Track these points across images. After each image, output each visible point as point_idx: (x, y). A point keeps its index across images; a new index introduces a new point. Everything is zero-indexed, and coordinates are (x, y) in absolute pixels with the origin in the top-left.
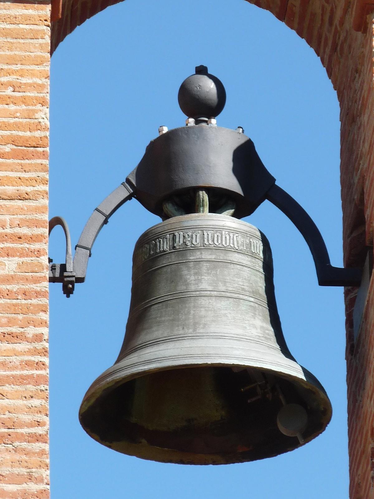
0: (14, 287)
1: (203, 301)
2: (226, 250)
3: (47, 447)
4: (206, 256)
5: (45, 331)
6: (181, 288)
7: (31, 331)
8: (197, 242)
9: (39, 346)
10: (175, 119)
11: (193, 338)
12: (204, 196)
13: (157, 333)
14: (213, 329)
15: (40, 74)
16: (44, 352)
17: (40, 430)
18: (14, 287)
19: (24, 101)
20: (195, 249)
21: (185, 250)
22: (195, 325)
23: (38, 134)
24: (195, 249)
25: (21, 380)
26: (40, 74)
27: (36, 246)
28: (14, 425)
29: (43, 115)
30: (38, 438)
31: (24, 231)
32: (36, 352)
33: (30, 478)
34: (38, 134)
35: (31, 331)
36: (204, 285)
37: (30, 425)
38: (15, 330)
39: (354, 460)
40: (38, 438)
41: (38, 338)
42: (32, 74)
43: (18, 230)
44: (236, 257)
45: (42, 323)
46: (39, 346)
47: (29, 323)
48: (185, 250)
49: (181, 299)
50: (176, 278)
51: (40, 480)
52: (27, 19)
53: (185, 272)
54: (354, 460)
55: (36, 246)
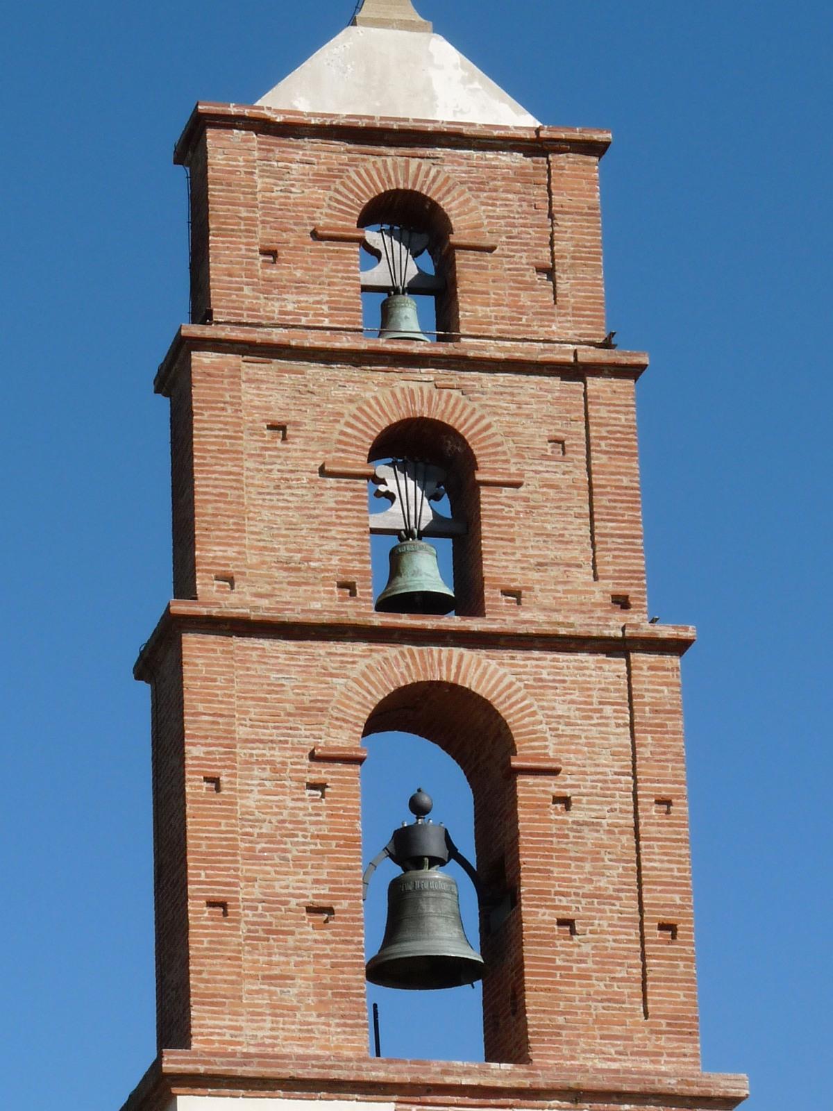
0: (347, 916)
1: (432, 919)
2: (441, 891)
3: (365, 1000)
4: (432, 894)
5: (363, 939)
6: (419, 911)
7: (356, 939)
8: (426, 887)
9: (360, 947)
10: (409, 819)
11: (428, 939)
12: (427, 860)
13: (408, 934)
14: (437, 934)
15: (357, 803)
16: (362, 950)
17: (362, 991)
18: (347, 916)
19: (349, 817)
20: (426, 890)
21: (420, 891)
22: (428, 932)
23: (356, 835)
24: (426, 890)
25: (353, 965)
26: (357, 803)
27: (357, 894)
28: (349, 988)
29: (359, 826)
30: (361, 995)
31: (351, 886)
32: (358, 950)
33: (359, 1017)
34: (356, 835)
35: (356, 939)
36: (431, 911)
37: (357, 989)
38: (348, 938)
39: (223, 836)
40: (361, 995)
41: (360, 943)
42: (353, 803)
43: (348, 886)
44: (445, 895)
45: (361, 935)
46: (360, 947)
47: (354, 935)
48: (420, 891)
49: (419, 918)
50: (416, 906)
51: (364, 1018)
52: (349, 774)
53: (424, 906)
54: (223, 836)
55: (357, 894)
